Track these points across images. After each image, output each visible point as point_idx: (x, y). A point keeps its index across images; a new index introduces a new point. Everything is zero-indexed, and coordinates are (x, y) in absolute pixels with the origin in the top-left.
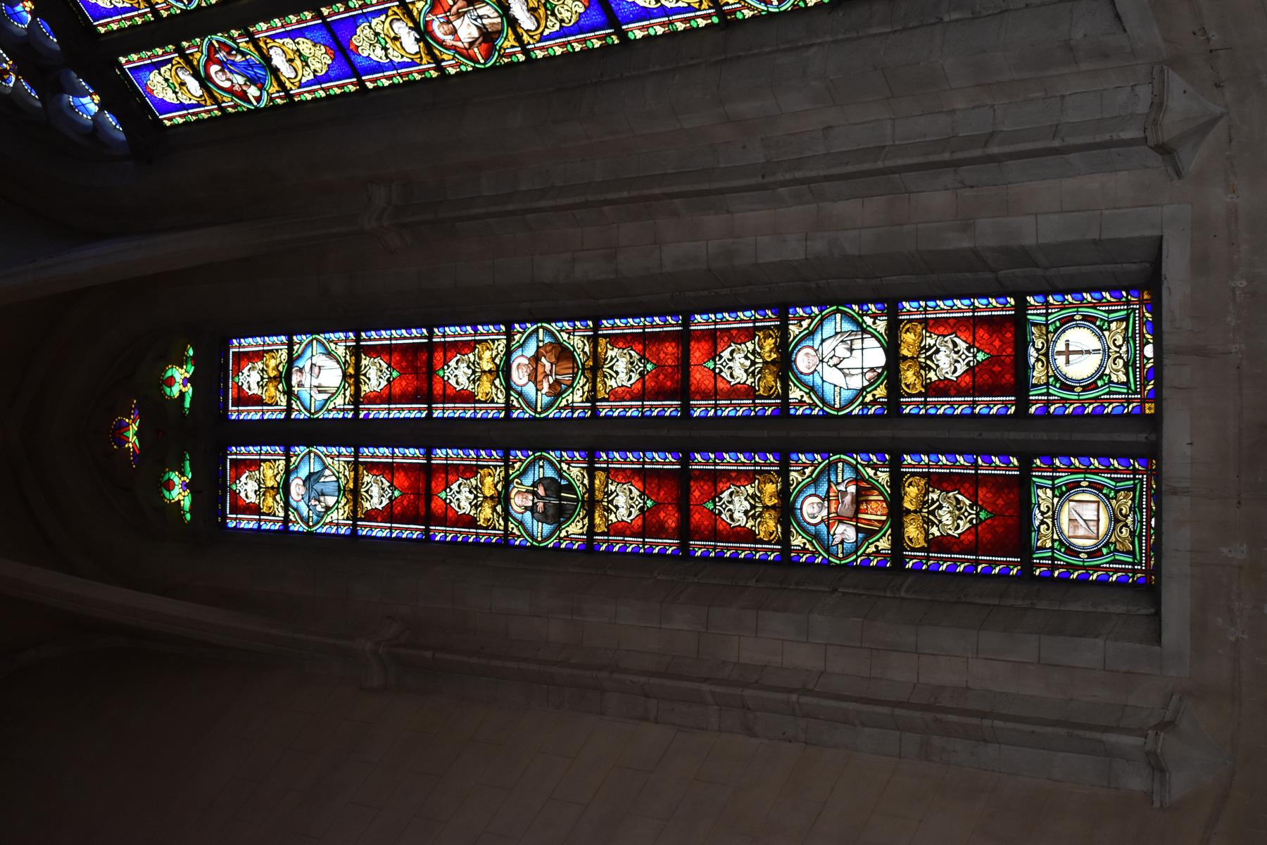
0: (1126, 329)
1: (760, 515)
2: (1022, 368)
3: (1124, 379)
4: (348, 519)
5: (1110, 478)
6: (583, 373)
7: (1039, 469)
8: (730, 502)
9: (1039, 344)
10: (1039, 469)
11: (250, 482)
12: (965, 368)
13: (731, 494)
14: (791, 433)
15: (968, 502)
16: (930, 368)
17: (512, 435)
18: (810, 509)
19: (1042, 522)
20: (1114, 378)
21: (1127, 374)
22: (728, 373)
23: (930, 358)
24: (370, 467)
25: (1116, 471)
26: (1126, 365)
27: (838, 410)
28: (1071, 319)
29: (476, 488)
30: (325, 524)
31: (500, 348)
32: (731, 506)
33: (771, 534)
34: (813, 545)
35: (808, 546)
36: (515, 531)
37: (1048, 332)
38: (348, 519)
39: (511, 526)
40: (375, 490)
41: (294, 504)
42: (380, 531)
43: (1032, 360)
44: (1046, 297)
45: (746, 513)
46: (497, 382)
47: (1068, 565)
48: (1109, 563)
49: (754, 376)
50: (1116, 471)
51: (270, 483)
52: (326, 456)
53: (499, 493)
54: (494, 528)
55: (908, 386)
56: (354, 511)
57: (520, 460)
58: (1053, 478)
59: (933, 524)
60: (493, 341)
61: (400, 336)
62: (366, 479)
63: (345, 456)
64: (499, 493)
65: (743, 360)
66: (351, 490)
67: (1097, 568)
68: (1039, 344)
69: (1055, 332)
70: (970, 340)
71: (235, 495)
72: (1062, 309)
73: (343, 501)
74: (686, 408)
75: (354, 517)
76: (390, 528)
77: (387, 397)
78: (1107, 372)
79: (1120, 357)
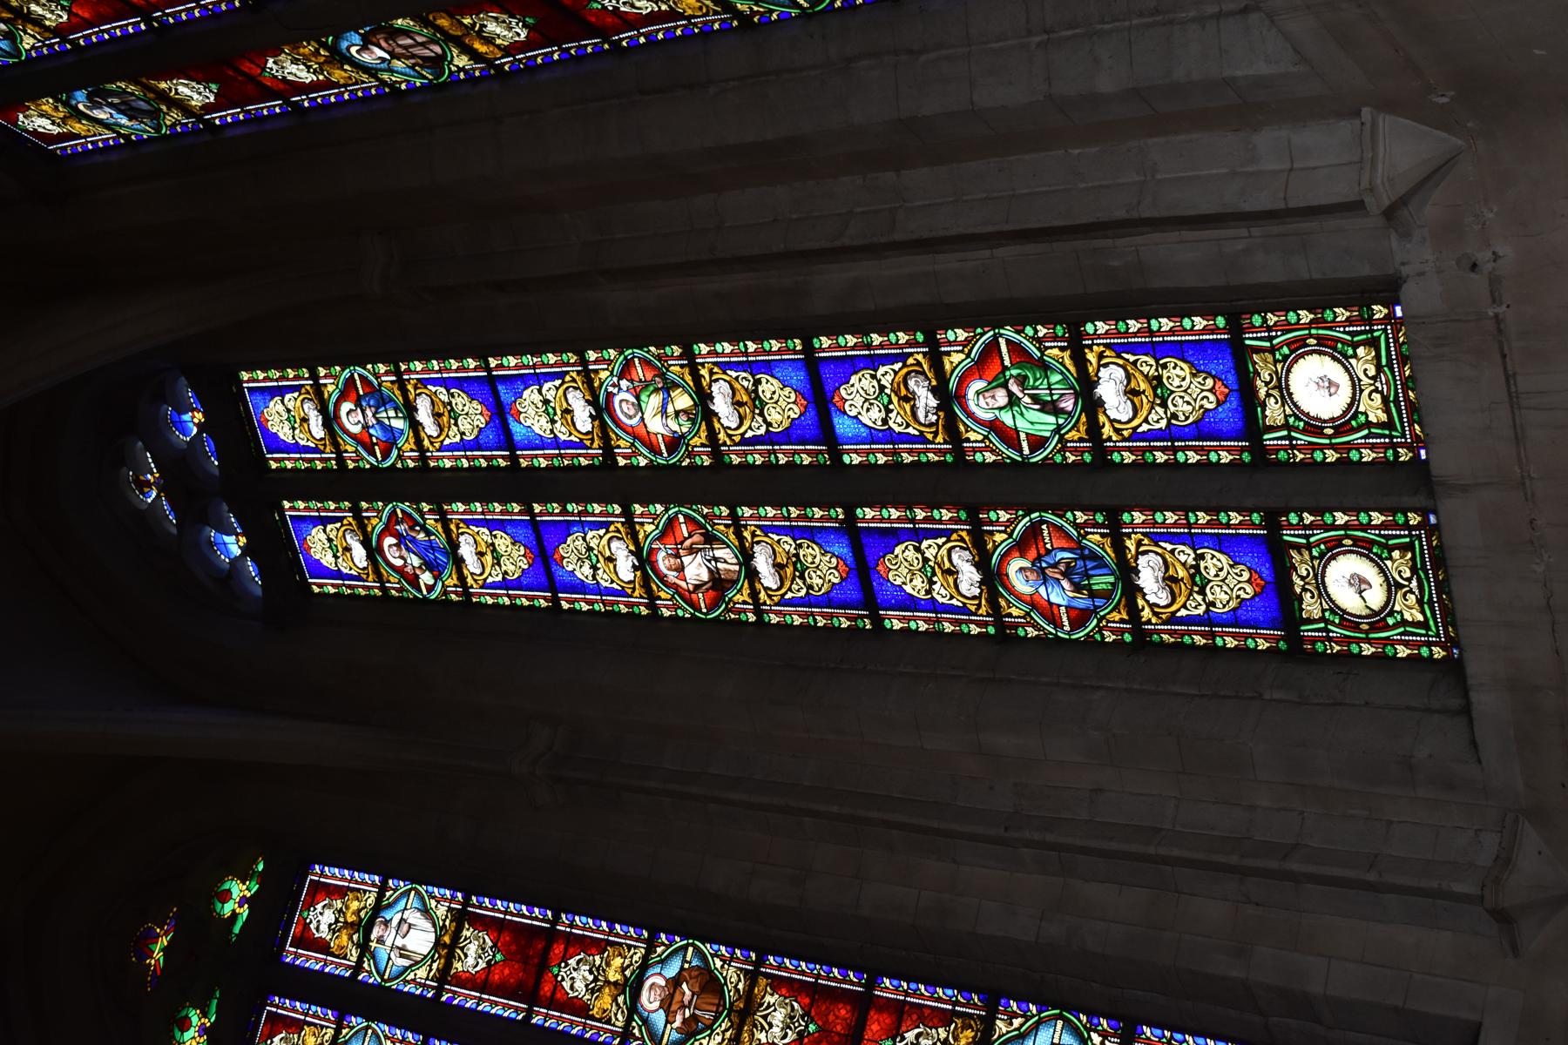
58: (1270, 339)
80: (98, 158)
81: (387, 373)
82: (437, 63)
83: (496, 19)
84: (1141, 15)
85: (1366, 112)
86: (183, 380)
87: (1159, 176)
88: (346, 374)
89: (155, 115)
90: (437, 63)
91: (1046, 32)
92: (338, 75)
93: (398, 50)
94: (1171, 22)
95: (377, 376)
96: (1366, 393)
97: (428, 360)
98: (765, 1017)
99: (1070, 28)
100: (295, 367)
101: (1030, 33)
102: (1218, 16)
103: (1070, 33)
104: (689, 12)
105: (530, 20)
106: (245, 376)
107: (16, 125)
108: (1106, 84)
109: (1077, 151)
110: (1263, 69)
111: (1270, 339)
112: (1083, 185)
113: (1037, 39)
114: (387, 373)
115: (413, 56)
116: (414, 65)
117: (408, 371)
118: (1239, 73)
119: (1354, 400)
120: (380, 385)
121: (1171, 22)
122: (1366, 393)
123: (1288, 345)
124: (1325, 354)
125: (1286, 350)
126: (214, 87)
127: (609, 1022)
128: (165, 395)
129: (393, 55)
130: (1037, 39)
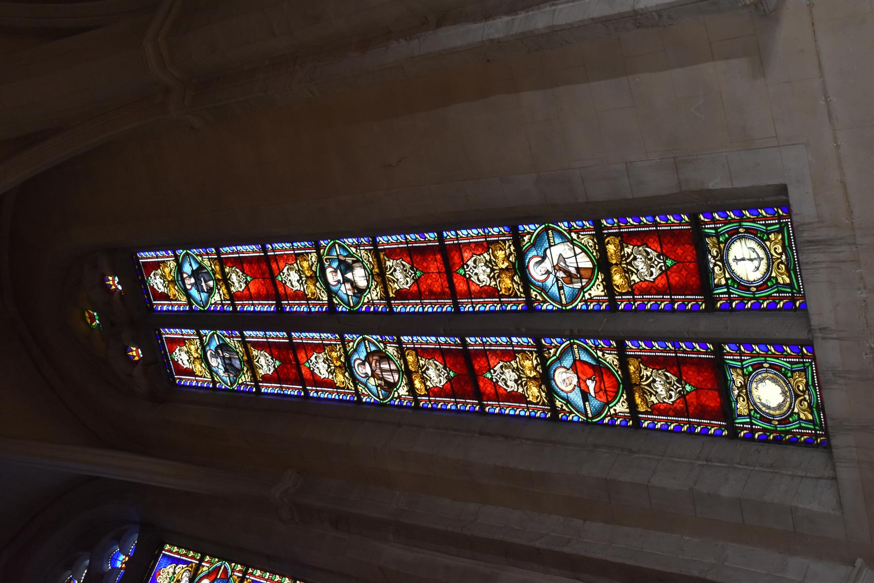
0: (783, 239)
1: (526, 384)
2: (706, 274)
3: (788, 281)
4: (381, 299)
5: (786, 362)
6: (373, 278)
7: (729, 354)
8: (502, 373)
9: (714, 252)
10: (729, 354)
11: (291, 273)
12: (659, 272)
13: (501, 367)
14: (537, 323)
15: (674, 378)
16: (632, 272)
17: (338, 320)
18: (564, 379)
19: (739, 395)
20: (781, 281)
21: (790, 277)
22: (476, 277)
23: (630, 264)
24: (392, 254)
25: (789, 356)
26: (788, 269)
27: (566, 306)
28: (736, 231)
29: (490, 261)
30: (364, 304)
31: (313, 259)
32: (503, 377)
33: (537, 398)
34: (568, 407)
35: (564, 407)
36: (539, 297)
37: (719, 242)
38: (381, 299)
39: (533, 294)
40: (399, 275)
41: (334, 288)
42: (269, 388)
43: (711, 266)
44: (612, 264)
45: (516, 381)
46: (318, 284)
47: (764, 430)
48: (796, 428)
49: (495, 280)
50: (789, 356)
51: (196, 355)
52: (349, 246)
53: (344, 363)
54: (348, 389)
55: (618, 287)
56: (386, 292)
57: (529, 233)
58: (741, 361)
59: (651, 394)
60: (307, 254)
61: (249, 250)
62: (389, 264)
63: (364, 245)
64: (513, 264)
65: (484, 268)
66: (377, 274)
67: (787, 432)
68: (714, 252)
69: (725, 242)
70: (659, 249)
71: (176, 363)
72: (726, 224)
73: (374, 283)
74: (456, 305)
75: (386, 296)
76: (422, 304)
77: (247, 296)
78: (774, 274)
79: (782, 262)
80: (194, 390)
81: (239, 571)
82: (390, 387)
83: (436, 366)
84: (762, 466)
85: (859, 562)
86: (136, 536)
87: (726, 564)
88: (219, 564)
89: (238, 372)
90: (390, 387)
91: (707, 460)
92: (340, 378)
93: (378, 372)
94: (776, 473)
95: (233, 570)
96: (776, 263)
97: (266, 571)
98: (391, 274)
99: (721, 462)
100: (195, 551)
101: (698, 458)
102: (806, 477)
103: (719, 464)
104: (531, 399)
105: (452, 374)
106: (167, 547)
107: (171, 353)
108: (725, 492)
109: (688, 538)
110: (815, 507)
111: (741, 361)
112: (681, 557)
113: (700, 463)
114: (239, 571)
115: (382, 379)
116: (379, 385)
117: (252, 574)
118: (800, 506)
119: (768, 270)
120: (231, 576)
121: (776, 473)
122: (776, 263)
123: (752, 366)
124: (764, 405)
125: (750, 369)
126: (278, 363)
127: (319, 299)
128: (120, 539)
129: (374, 375)
130: (700, 463)
